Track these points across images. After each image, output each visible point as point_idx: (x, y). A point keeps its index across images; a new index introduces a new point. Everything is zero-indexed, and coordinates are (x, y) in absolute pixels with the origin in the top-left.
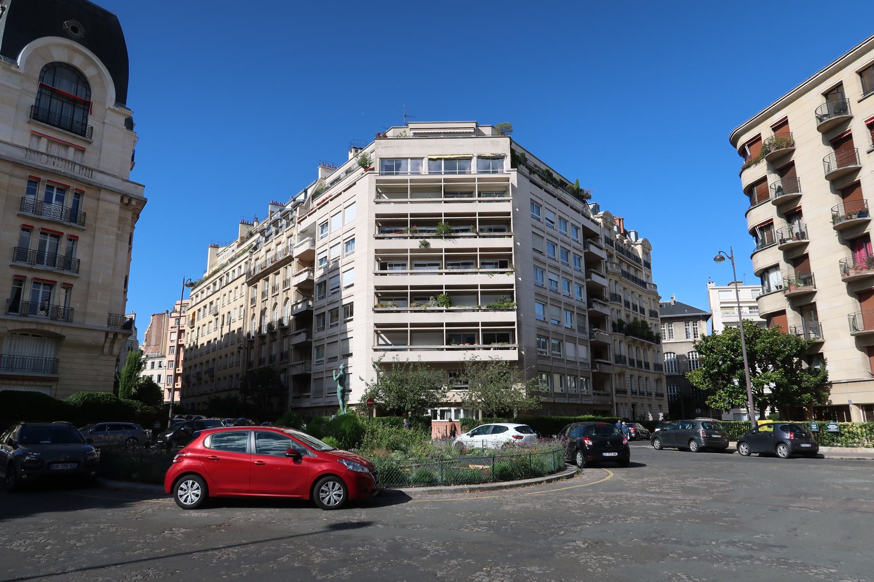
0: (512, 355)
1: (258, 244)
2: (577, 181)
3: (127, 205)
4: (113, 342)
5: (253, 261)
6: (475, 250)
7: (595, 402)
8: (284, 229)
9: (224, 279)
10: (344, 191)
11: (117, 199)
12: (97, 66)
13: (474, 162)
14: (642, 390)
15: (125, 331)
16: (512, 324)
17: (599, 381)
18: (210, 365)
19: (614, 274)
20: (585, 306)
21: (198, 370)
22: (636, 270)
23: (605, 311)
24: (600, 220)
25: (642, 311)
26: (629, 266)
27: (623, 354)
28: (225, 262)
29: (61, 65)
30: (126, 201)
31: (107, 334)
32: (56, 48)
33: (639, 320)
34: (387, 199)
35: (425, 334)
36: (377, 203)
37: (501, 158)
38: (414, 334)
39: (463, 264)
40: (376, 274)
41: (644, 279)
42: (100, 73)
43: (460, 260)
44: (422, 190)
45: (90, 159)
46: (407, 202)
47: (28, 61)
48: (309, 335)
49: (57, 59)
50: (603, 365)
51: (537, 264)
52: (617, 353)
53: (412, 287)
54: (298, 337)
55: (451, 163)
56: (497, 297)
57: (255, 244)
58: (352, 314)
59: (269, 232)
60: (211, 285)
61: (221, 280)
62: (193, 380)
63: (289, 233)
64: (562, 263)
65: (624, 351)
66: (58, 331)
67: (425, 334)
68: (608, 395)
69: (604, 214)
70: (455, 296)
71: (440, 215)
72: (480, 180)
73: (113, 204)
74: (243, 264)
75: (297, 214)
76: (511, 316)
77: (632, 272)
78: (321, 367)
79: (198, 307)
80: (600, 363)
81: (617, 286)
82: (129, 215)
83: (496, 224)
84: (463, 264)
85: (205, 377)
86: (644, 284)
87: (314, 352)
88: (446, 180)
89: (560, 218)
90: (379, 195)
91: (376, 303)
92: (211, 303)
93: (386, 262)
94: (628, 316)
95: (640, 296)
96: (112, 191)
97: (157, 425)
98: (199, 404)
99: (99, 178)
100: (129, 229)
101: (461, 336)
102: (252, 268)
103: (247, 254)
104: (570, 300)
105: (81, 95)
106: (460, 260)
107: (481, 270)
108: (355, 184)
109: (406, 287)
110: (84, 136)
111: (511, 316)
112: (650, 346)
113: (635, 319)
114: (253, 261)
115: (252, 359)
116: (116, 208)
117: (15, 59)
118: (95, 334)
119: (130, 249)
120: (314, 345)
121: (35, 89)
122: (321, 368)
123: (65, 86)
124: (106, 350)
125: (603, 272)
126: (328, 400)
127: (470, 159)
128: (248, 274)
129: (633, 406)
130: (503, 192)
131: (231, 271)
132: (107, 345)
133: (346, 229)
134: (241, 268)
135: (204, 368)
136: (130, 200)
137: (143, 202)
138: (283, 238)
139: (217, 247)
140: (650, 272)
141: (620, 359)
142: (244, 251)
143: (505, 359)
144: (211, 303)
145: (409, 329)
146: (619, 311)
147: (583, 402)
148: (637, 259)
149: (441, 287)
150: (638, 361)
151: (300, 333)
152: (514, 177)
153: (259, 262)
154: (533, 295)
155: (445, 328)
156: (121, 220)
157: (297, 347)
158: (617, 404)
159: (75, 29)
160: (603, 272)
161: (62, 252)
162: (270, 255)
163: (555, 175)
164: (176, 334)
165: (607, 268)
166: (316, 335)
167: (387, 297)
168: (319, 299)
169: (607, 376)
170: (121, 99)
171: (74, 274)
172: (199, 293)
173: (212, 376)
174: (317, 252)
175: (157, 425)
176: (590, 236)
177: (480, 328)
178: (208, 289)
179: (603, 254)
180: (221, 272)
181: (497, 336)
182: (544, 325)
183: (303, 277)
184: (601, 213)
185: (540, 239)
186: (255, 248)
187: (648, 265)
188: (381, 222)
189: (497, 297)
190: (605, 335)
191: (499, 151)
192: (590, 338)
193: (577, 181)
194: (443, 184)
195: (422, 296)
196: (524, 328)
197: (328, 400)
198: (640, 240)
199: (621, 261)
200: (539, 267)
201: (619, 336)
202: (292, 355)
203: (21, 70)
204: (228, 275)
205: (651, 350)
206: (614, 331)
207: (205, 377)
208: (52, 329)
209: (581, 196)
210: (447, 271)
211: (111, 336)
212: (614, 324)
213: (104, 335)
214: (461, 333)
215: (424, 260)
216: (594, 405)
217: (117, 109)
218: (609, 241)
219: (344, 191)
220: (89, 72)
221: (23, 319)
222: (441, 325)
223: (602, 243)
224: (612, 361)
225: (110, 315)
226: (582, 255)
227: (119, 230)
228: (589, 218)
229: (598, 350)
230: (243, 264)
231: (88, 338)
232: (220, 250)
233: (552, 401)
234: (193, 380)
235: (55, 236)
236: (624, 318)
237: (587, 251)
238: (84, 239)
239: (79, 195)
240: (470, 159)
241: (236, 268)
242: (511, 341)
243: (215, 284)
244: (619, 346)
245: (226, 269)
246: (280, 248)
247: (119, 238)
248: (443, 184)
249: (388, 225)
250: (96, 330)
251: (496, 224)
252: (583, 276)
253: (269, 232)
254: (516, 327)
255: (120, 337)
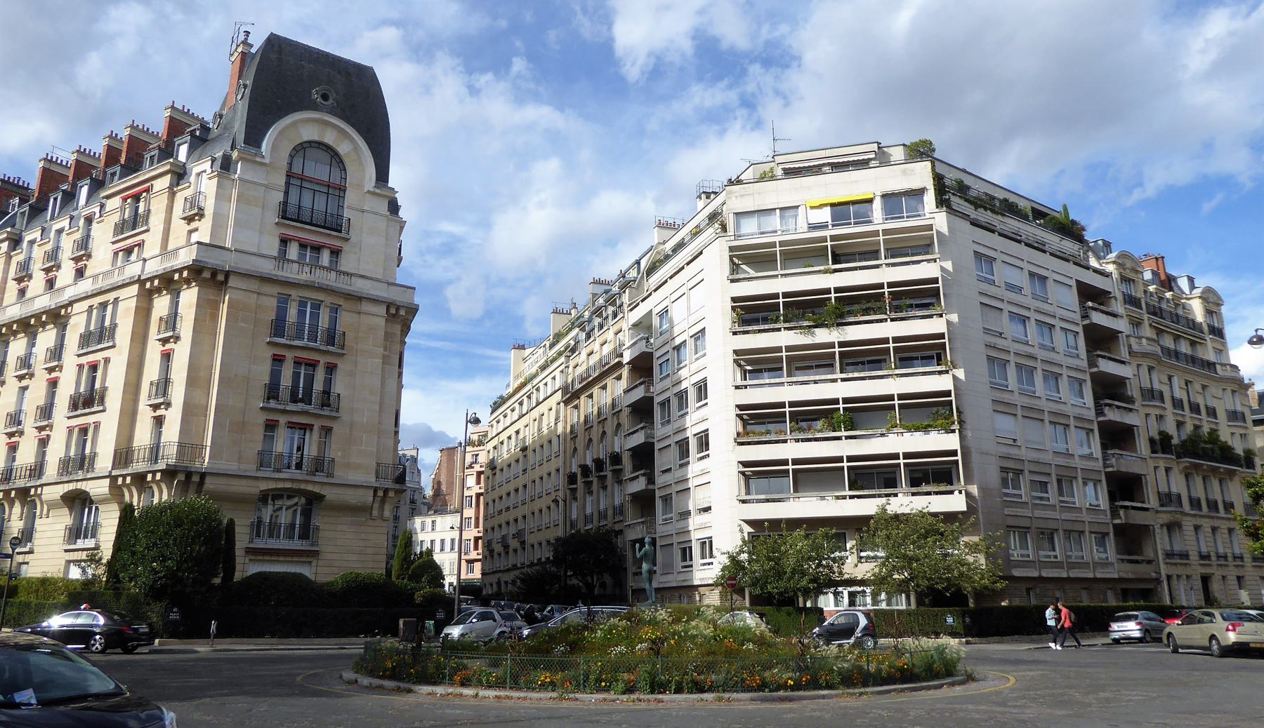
0: (955, 502)
1: (577, 343)
2: (1065, 208)
3: (394, 315)
4: (383, 500)
5: (571, 369)
6: (886, 341)
7: (1124, 576)
8: (611, 322)
9: (534, 397)
10: (671, 277)
11: (382, 310)
12: (352, 140)
13: (877, 205)
14: (1221, 551)
15: (398, 486)
16: (954, 453)
17: (1131, 539)
18: (521, 525)
19: (1145, 355)
20: (1091, 414)
21: (504, 532)
22: (1193, 344)
23: (1130, 419)
24: (1111, 268)
25: (1212, 412)
26: (1177, 338)
27: (1174, 490)
28: (533, 370)
29: (311, 144)
30: (393, 311)
31: (376, 490)
32: (304, 126)
33: (1206, 429)
34: (752, 273)
35: (812, 476)
36: (732, 281)
37: (920, 192)
38: (799, 475)
39: (869, 362)
40: (737, 387)
41: (1211, 356)
42: (356, 149)
43: (864, 358)
44: (802, 254)
45: (346, 263)
46: (776, 276)
47: (274, 148)
48: (651, 480)
49: (306, 139)
50: (1133, 512)
51: (994, 354)
52: (1163, 488)
53: (792, 404)
54: (635, 482)
55: (841, 210)
56: (926, 411)
57: (572, 343)
58: (707, 449)
59: (591, 326)
60: (517, 405)
61: (529, 397)
62: (498, 548)
63: (616, 328)
64: (1043, 347)
65: (1177, 485)
66: (316, 489)
67: (812, 476)
68: (1149, 562)
69: (1118, 257)
70: (860, 415)
71: (828, 291)
72: (886, 232)
73: (376, 318)
74: (557, 373)
75: (626, 298)
76: (950, 441)
77: (1184, 348)
78: (669, 527)
79: (506, 434)
80: (1126, 507)
81: (1155, 376)
82: (397, 329)
83: (919, 297)
84: (869, 362)
85: (514, 544)
86: (1211, 366)
87: (659, 504)
88: (833, 238)
89: (1032, 274)
90: (735, 268)
91: (741, 429)
92: (517, 432)
93: (755, 365)
94: (1180, 424)
95: (1204, 387)
96: (375, 301)
97: (440, 615)
98: (506, 583)
99: (359, 286)
100: (397, 347)
101: (872, 476)
102: (570, 380)
103: (562, 359)
104: (1061, 407)
105: (336, 179)
106: (864, 358)
107: (897, 372)
108: (701, 253)
109: (782, 405)
110: (340, 231)
111: (950, 441)
112: (1231, 474)
113: (1197, 427)
114: (571, 369)
115: (574, 516)
116: (382, 322)
117: (259, 147)
118: (361, 492)
119: (400, 374)
120: (658, 494)
121: (281, 180)
122: (670, 529)
123: (318, 170)
124: (375, 513)
125: (1124, 354)
126: (681, 577)
127: (870, 201)
128: (565, 389)
129: (1206, 580)
130: (926, 247)
131: (541, 385)
132: (376, 505)
133: (692, 320)
134: (554, 381)
135: (512, 530)
136: (398, 308)
137: (413, 310)
138: (610, 335)
139: (522, 347)
140: (1224, 344)
141: (1167, 499)
142: (560, 354)
143: (933, 509)
144: (517, 432)
145: (790, 467)
146: (1160, 418)
147: (1099, 575)
148: (1193, 324)
149: (836, 401)
150: (1208, 501)
151: (637, 477)
152: (941, 221)
153: (580, 370)
154: (989, 405)
155: (845, 464)
156: (388, 336)
157: (636, 497)
158: (1169, 577)
159: (325, 97)
160: (1124, 354)
161: (318, 386)
162: (594, 359)
163: (1022, 204)
164: (474, 477)
165: (1130, 346)
166: (660, 480)
167: (756, 420)
168: (663, 424)
169: (1145, 530)
170: (382, 175)
171: (334, 414)
172: (501, 417)
173: (523, 543)
174: (657, 354)
175: (440, 615)
176: (1090, 295)
177: (902, 461)
178: (513, 410)
179: (1121, 325)
180: (529, 387)
181: (931, 473)
182: (1013, 452)
183: (639, 393)
184: (1112, 256)
185: (998, 312)
186: (573, 350)
187: (1218, 332)
188: (742, 308)
189: (926, 411)
190: (1140, 460)
191: (916, 185)
192: (1105, 466)
193: (1065, 208)
194: (829, 243)
195: (808, 417)
196: (975, 458)
197: (681, 577)
198: (1197, 292)
199: (1160, 332)
200: (996, 362)
201: (1162, 461)
202: (629, 510)
203: (267, 161)
204: (538, 390)
205: (1237, 479)
206: (1153, 452)
207: (514, 544)
208: (310, 488)
209: (1071, 230)
210: (844, 376)
211: (380, 493)
212: (1152, 441)
213: (371, 493)
214: (874, 471)
215: (809, 362)
216: (1121, 580)
217: (378, 191)
218: (1131, 301)
219: (671, 277)
220: (343, 148)
221: (277, 475)
222: (840, 459)
223: (1118, 307)
224: (1153, 502)
225: (378, 464)
226: (1080, 329)
227: (385, 350)
228: (1088, 268)
229: (1124, 487)
230: (557, 373)
231: (352, 497)
232: (528, 351)
233: (1036, 574)
234: (498, 548)
235: (310, 365)
236: (1171, 428)
237: (1087, 322)
238: (343, 366)
239: (335, 310)
240: (870, 201)
241: (549, 379)
242: (955, 481)
243: (521, 404)
244: (1163, 477)
245: (535, 381)
246: (607, 349)
247: (386, 361)
248: (829, 243)
249: (751, 313)
250: (362, 486)
251: (919, 297)
252: (1084, 364)
253: (591, 326)
254: (959, 458)
255: (391, 494)
